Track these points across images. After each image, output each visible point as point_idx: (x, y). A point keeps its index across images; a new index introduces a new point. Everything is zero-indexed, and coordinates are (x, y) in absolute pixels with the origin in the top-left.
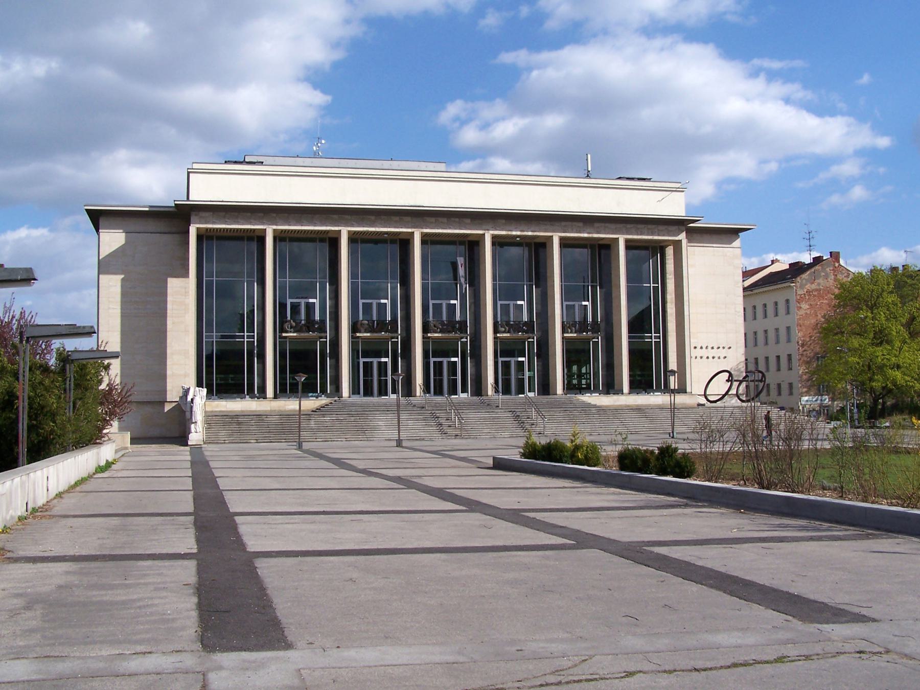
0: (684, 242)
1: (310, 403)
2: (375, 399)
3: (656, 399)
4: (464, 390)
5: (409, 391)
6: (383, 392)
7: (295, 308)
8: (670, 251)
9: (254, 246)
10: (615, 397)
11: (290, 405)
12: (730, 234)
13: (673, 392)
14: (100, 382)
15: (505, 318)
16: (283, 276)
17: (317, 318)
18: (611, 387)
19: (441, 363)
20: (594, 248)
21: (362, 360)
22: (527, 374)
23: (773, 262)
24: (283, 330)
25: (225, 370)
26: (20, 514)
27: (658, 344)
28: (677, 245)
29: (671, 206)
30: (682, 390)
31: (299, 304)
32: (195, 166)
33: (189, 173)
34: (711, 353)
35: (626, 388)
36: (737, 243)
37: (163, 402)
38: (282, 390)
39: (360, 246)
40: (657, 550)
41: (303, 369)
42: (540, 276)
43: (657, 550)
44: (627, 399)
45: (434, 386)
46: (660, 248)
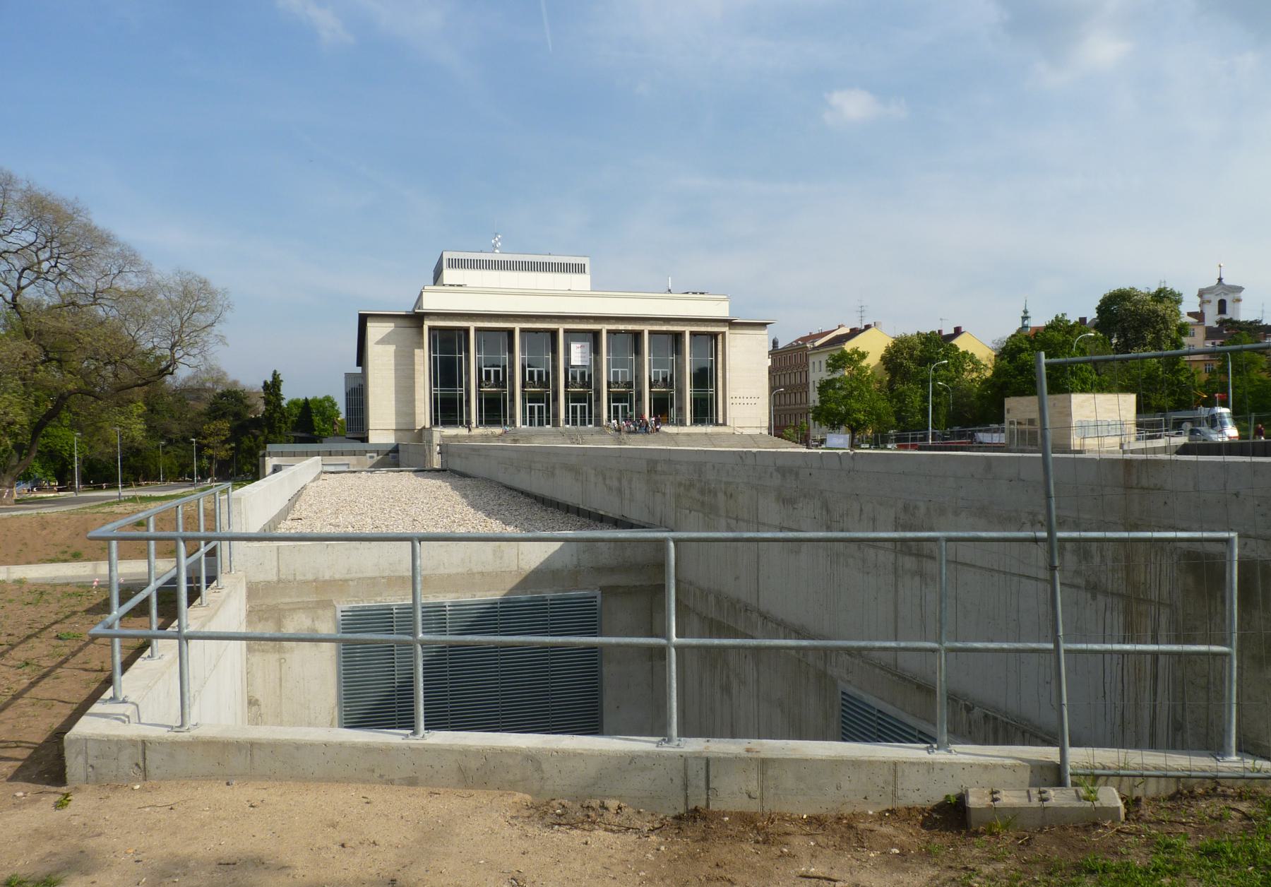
1: (498, 430)
2: (536, 428)
3: (710, 429)
5: (556, 424)
8: (720, 337)
15: (625, 373)
16: (435, 352)
18: (682, 423)
26: (35, 825)
28: (724, 334)
29: (717, 308)
30: (724, 424)
33: (363, 320)
34: (746, 401)
35: (688, 422)
36: (766, 332)
40: (510, 530)
42: (638, 350)
43: (510, 530)
44: (689, 429)
45: (572, 419)
46: (714, 336)
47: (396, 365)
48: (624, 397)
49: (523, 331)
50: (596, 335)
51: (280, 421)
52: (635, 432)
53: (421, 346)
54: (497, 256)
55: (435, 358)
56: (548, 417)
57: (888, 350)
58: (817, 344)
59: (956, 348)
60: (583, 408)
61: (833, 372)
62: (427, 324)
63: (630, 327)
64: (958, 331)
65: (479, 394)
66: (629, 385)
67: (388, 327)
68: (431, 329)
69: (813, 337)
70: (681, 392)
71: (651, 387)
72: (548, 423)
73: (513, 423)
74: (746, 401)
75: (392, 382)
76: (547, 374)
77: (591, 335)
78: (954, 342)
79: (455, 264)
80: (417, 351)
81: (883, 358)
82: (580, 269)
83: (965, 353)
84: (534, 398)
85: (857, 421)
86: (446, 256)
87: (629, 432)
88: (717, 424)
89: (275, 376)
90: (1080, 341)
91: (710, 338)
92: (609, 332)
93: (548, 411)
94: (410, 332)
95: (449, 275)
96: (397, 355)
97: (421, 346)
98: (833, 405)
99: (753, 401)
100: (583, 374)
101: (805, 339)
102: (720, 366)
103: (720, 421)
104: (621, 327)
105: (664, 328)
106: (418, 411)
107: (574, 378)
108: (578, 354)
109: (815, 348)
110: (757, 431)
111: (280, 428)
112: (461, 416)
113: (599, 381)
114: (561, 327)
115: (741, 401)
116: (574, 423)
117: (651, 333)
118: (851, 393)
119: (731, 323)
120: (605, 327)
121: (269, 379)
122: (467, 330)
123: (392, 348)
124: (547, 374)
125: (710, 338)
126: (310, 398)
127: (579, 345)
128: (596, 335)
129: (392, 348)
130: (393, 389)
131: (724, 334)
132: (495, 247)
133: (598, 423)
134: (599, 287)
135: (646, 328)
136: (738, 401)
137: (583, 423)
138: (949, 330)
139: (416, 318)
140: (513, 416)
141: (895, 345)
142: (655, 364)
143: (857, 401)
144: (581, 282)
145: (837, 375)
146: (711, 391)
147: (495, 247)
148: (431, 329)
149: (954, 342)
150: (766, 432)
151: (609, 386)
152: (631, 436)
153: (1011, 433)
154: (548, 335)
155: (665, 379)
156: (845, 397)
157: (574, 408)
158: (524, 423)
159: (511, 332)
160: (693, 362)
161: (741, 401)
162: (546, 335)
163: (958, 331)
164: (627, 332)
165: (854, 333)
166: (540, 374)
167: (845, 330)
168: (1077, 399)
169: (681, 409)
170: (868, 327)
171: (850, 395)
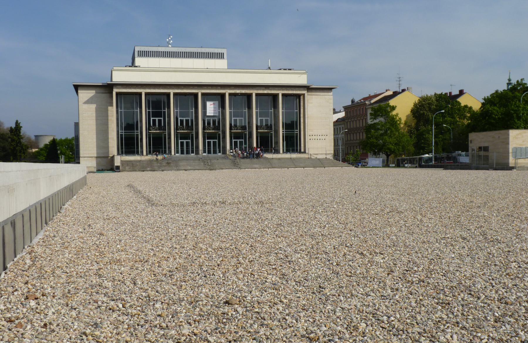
0: (306, 95)
3: (294, 156)
4: (220, 152)
5: (197, 153)
6: (188, 153)
7: (182, 121)
8: (302, 97)
9: (138, 97)
10: (277, 155)
11: (288, 156)
12: (330, 89)
13: (303, 153)
14: (469, 123)
15: (241, 121)
16: (149, 109)
17: (163, 125)
18: (277, 151)
19: (155, 120)
20: (269, 98)
21: (207, 141)
22: (244, 146)
23: (387, 91)
24: (149, 130)
25: (128, 145)
27: (137, 135)
28: (304, 95)
29: (301, 79)
31: (155, 120)
32: (114, 68)
34: (319, 137)
36: (331, 94)
37: (108, 157)
38: (149, 153)
39: (178, 97)
41: (158, 144)
42: (275, 105)
46: (298, 96)
47: (97, 117)
48: (240, 135)
49: (175, 94)
50: (223, 96)
51: (20, 152)
52: (247, 157)
53: (112, 105)
54: (170, 49)
55: (149, 112)
56: (192, 148)
57: (415, 105)
58: (372, 101)
59: (460, 104)
60: (214, 143)
61: (375, 119)
62: (115, 91)
63: (243, 91)
64: (461, 93)
65: (149, 136)
66: (244, 128)
67: (91, 93)
68: (118, 94)
69: (370, 97)
70: (277, 132)
71: (257, 129)
72: (193, 152)
73: (170, 152)
74: (319, 137)
75: (94, 127)
76: (192, 121)
77: (219, 97)
78: (458, 100)
79: (143, 54)
80: (110, 108)
81: (412, 111)
82: (220, 56)
83: (466, 106)
84: (184, 137)
85: (389, 149)
86: (137, 49)
87: (244, 158)
88: (300, 152)
89: (17, 124)
90: (525, 96)
91: (294, 98)
92: (230, 94)
93: (245, 144)
94: (105, 96)
95: (139, 61)
96: (97, 110)
97: (112, 105)
98: (375, 141)
99: (323, 137)
100: (214, 122)
101: (365, 99)
102: (302, 115)
103: (302, 150)
104: (238, 91)
105: (266, 92)
106: (110, 145)
107: (209, 123)
108: (211, 108)
109: (371, 104)
110: (323, 157)
111: (20, 156)
112: (138, 148)
113: (250, 127)
114: (200, 92)
115: (316, 137)
116: (209, 152)
117: (257, 95)
118: (386, 132)
119: (308, 88)
120: (227, 92)
121: (14, 126)
122: (278, 94)
123: (94, 106)
124: (192, 121)
125: (294, 98)
126: (58, 138)
127: (212, 103)
128: (223, 96)
129: (94, 106)
130: (95, 131)
131: (304, 95)
132: (168, 43)
133: (224, 152)
134: (232, 67)
135: (254, 92)
136: (314, 137)
137: (215, 152)
138: (455, 92)
139: (109, 87)
140: (170, 148)
141: (420, 102)
142: (260, 114)
143: (390, 137)
144: (222, 64)
145: (377, 121)
146: (296, 131)
147: (168, 43)
148: (118, 94)
149: (458, 100)
150: (332, 158)
151: (231, 128)
152: (242, 160)
153: (473, 156)
154: (245, 97)
155: (267, 125)
156: (382, 135)
157: (209, 143)
158: (205, 152)
159: (196, 95)
160: (286, 115)
161: (316, 137)
162: (190, 96)
163: (461, 93)
164: (242, 94)
165: (395, 94)
166: (187, 121)
167: (390, 93)
168: (513, 133)
169: (277, 143)
170: (403, 91)
171: (386, 133)
